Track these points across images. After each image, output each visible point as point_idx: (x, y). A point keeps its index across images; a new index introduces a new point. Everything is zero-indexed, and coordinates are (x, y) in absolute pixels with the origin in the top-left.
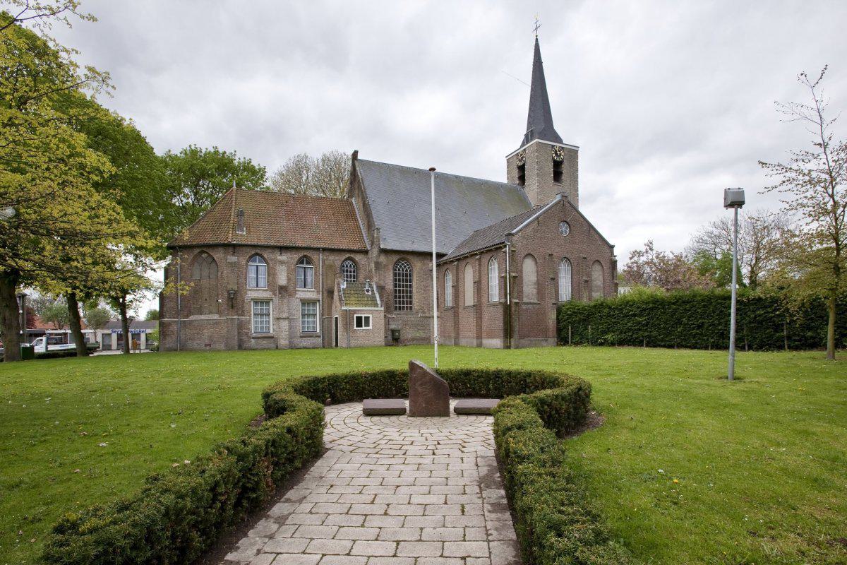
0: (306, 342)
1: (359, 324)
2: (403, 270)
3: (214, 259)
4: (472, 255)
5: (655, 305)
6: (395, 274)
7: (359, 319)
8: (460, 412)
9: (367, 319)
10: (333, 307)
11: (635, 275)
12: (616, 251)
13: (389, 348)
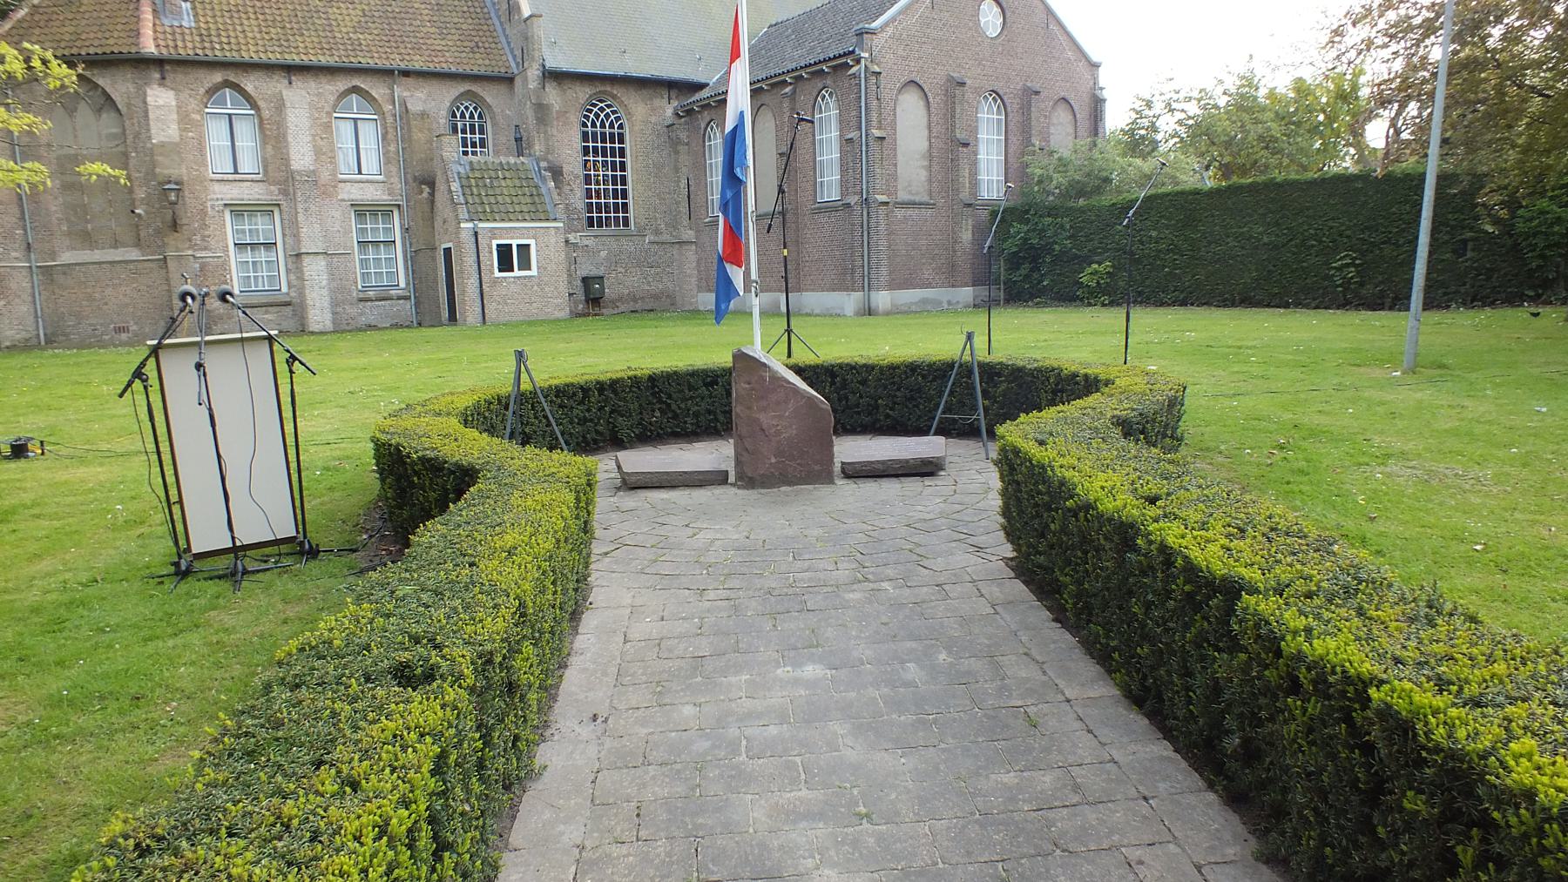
0: (370, 313)
1: (505, 263)
2: (594, 125)
3: (108, 98)
4: (773, 85)
5: (1178, 209)
6: (585, 137)
7: (505, 253)
8: (856, 473)
9: (524, 249)
10: (438, 223)
11: (1138, 143)
12: (1104, 78)
13: (580, 320)
